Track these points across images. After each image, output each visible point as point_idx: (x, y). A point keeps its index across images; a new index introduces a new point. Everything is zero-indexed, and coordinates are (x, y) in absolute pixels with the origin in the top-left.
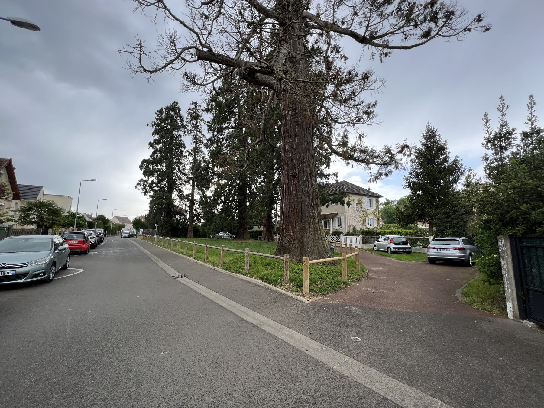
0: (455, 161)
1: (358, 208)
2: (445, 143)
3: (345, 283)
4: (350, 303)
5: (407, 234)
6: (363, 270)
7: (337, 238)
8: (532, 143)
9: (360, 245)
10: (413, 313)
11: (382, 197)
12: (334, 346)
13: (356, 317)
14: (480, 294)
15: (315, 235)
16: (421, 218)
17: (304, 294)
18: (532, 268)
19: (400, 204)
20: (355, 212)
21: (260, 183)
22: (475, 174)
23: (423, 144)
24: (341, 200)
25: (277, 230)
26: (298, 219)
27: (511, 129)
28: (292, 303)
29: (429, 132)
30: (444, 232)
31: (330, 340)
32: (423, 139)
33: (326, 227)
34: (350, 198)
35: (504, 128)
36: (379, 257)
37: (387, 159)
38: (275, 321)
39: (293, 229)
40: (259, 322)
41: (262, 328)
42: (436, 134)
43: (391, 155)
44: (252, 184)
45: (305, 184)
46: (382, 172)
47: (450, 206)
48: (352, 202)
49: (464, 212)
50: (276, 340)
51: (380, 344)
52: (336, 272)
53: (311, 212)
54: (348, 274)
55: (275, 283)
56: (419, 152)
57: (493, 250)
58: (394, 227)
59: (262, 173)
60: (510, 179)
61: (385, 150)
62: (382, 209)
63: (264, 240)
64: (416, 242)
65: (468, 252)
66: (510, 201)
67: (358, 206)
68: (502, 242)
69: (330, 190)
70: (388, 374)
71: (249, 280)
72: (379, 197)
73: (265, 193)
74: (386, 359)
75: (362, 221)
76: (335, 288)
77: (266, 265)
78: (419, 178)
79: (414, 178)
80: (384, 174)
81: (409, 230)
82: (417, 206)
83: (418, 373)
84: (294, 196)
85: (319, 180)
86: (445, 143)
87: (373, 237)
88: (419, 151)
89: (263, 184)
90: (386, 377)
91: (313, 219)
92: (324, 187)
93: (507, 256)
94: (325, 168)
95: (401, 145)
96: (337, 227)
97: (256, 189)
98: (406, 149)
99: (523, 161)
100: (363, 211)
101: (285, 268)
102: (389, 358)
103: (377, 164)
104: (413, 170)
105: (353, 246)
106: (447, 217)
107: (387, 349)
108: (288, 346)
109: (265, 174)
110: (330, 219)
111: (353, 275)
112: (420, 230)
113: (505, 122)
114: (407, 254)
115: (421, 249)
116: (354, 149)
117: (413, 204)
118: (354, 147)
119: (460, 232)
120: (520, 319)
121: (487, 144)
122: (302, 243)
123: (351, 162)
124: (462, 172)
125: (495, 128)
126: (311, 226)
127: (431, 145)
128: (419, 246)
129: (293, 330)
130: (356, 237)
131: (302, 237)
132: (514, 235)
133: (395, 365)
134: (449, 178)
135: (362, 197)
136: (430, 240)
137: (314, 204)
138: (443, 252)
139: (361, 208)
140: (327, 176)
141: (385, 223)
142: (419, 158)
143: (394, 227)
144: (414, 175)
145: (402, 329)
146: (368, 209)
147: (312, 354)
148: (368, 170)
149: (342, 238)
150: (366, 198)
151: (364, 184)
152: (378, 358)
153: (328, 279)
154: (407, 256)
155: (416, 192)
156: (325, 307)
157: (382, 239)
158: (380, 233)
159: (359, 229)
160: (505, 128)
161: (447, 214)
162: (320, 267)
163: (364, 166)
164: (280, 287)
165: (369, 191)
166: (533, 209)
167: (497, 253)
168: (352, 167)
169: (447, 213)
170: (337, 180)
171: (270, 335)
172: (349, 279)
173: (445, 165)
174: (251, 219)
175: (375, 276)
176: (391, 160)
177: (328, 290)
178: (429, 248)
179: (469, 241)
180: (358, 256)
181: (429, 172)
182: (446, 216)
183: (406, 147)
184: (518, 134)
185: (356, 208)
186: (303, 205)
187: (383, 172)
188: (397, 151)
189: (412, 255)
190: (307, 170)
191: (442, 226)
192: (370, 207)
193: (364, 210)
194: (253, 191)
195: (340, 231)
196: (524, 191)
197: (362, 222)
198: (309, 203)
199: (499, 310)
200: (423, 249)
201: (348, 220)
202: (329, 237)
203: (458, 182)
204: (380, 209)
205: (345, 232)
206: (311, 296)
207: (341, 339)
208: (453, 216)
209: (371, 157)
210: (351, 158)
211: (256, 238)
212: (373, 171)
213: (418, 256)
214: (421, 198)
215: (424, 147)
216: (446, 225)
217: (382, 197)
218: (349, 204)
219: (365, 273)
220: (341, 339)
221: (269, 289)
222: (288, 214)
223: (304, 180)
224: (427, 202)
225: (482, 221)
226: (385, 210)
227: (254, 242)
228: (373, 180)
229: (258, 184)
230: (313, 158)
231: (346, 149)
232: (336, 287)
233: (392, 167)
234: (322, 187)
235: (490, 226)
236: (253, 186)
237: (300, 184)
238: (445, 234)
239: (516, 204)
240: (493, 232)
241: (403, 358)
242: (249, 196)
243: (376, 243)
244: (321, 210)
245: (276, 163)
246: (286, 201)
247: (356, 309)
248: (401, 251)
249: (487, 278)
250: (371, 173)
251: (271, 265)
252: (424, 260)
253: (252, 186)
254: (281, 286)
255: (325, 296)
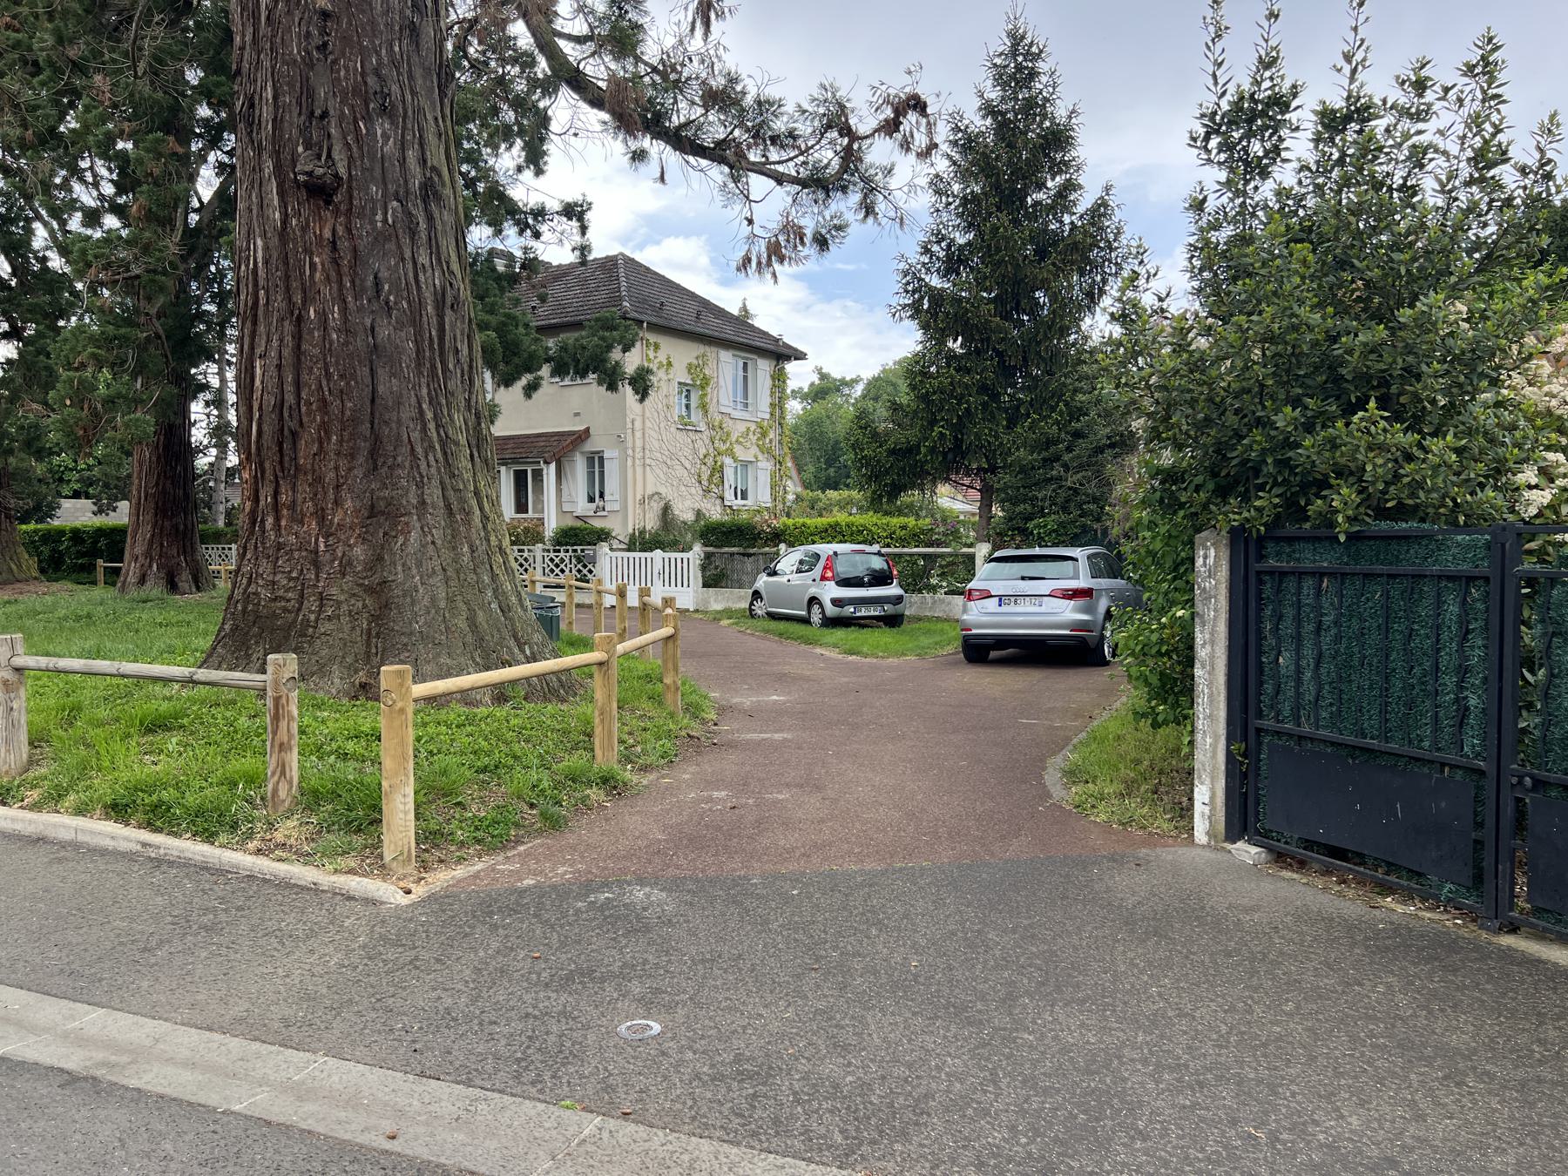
0: (1100, 206)
1: (688, 407)
2: (1070, 117)
3: (608, 782)
4: (624, 871)
5: (891, 538)
6: (693, 710)
7: (579, 560)
8: (1341, 162)
9: (688, 596)
10: (884, 873)
11: (800, 356)
12: (533, 1083)
13: (647, 929)
14: (1121, 766)
15: (454, 548)
16: (950, 464)
17: (388, 858)
18: (1279, 653)
19: (876, 399)
20: (673, 429)
21: (92, 218)
22: (1153, 272)
23: (989, 109)
24: (604, 361)
25: (229, 524)
26: (352, 456)
27: (1286, 87)
28: (317, 915)
29: (1014, 52)
30: (1030, 525)
31: (518, 1061)
32: (989, 83)
33: (521, 507)
34: (651, 354)
35: (1267, 74)
36: (770, 645)
37: (827, 156)
38: (210, 1029)
39: (320, 514)
40: (100, 1056)
41: (125, 1082)
42: (1042, 66)
43: (846, 141)
44: (28, 220)
45: (391, 246)
46: (802, 222)
47: (1061, 411)
48: (661, 374)
49: (1109, 438)
50: (212, 1127)
51: (744, 1028)
52: (566, 732)
53: (429, 415)
54: (626, 737)
55: (208, 824)
56: (967, 143)
57: (1176, 589)
58: (842, 508)
59: (105, 150)
60: (1259, 302)
61: (822, 110)
62: (799, 417)
63: (142, 580)
64: (926, 573)
65: (1103, 604)
66: (1249, 391)
67: (688, 397)
68: (1205, 557)
69: (543, 299)
70: (765, 1145)
71: (29, 830)
72: (788, 358)
73: (130, 285)
74: (764, 1084)
75: (705, 477)
76: (557, 808)
77: (150, 731)
78: (958, 274)
79: (938, 271)
80: (809, 233)
81: (903, 520)
82: (941, 410)
83: (879, 1110)
84: (323, 316)
85: (479, 236)
86: (1070, 117)
87: (749, 555)
88: (970, 140)
89: (111, 221)
90: (756, 1160)
91: (445, 453)
92: (513, 279)
93: (1216, 610)
94: (519, 169)
95: (892, 91)
96: (582, 507)
97: (64, 251)
98: (912, 117)
99: (1306, 233)
100: (712, 428)
101: (275, 733)
102: (774, 1077)
103: (780, 179)
104: (939, 232)
105: (656, 599)
106: (1048, 462)
107: (769, 1043)
108: (284, 1140)
109: (123, 157)
110: (546, 462)
111: (648, 735)
112: (944, 516)
113: (1273, 49)
114: (886, 624)
115: (943, 601)
116: (673, 76)
117: (925, 398)
118: (674, 70)
119: (1084, 526)
120: (1225, 841)
121: (1207, 138)
122: (379, 590)
123: (657, 149)
124: (1117, 264)
125: (1240, 76)
126: (433, 494)
127: (1016, 115)
128: (933, 589)
129: (314, 1052)
130: (673, 555)
131: (380, 559)
132: (1244, 530)
133: (798, 1101)
134: (1071, 287)
135: (711, 351)
136: (979, 561)
137: (445, 369)
138: (1019, 609)
139: (704, 407)
140: (530, 220)
141: (806, 488)
142: (964, 175)
143: (843, 505)
144: (938, 258)
145: (835, 948)
146: (736, 414)
147: (421, 1151)
148: (738, 207)
149: (607, 560)
150: (726, 356)
151: (725, 283)
152: (729, 1089)
153: (518, 772)
154: (884, 636)
155: (941, 342)
156: (500, 910)
157: (789, 560)
158: (783, 532)
159: (689, 517)
160: (1271, 79)
161: (1047, 449)
162: (482, 711)
163: (720, 179)
164: (241, 846)
165: (742, 321)
166: (1309, 428)
167: (1187, 601)
168: (662, 178)
169: (1050, 442)
170: (584, 249)
171: (175, 1109)
172: (627, 759)
173: (1061, 222)
174: (41, 454)
175: (749, 731)
176: (844, 168)
177: (517, 825)
178: (969, 595)
179: (1110, 566)
180: (675, 647)
181: (998, 250)
182: (1045, 454)
183: (915, 108)
184: (1304, 115)
185: (678, 410)
186: (382, 374)
187: (809, 225)
188: (874, 124)
189: (904, 631)
190: (403, 161)
191: (1024, 502)
192: (746, 405)
193: (718, 418)
194: (45, 269)
195: (597, 524)
196: (1293, 354)
197: (705, 483)
198: (419, 365)
199: (1171, 820)
200: (949, 603)
201: (639, 470)
202: (539, 559)
203: (1101, 305)
204: (790, 419)
205: (621, 529)
206: (424, 866)
207: (568, 1044)
208: (1067, 457)
209: (757, 134)
210: (655, 125)
211: (83, 573)
212: (759, 212)
213: (928, 632)
214: (958, 370)
215: (989, 121)
216: (1040, 496)
217: (800, 356)
218: (641, 384)
219: (704, 722)
220: (568, 1044)
221: (171, 864)
222: (291, 424)
223: (385, 220)
224: (983, 388)
225: (1159, 471)
226: (811, 424)
227: (67, 597)
228: (759, 263)
229: (75, 223)
230: (442, 95)
231: (631, 68)
232: (559, 803)
233: (845, 205)
234: (499, 278)
235: (1177, 494)
236: (40, 237)
237: (362, 244)
238: (1032, 533)
239: (1264, 407)
240: (1184, 518)
241: (831, 1068)
242: (9, 300)
243: (762, 581)
244: (493, 412)
245: (204, 92)
246: (275, 343)
247: (648, 896)
248: (863, 612)
249: (1149, 701)
250: (750, 222)
251: (182, 727)
252: (950, 649)
253: (30, 232)
254: (250, 835)
255: (500, 858)
